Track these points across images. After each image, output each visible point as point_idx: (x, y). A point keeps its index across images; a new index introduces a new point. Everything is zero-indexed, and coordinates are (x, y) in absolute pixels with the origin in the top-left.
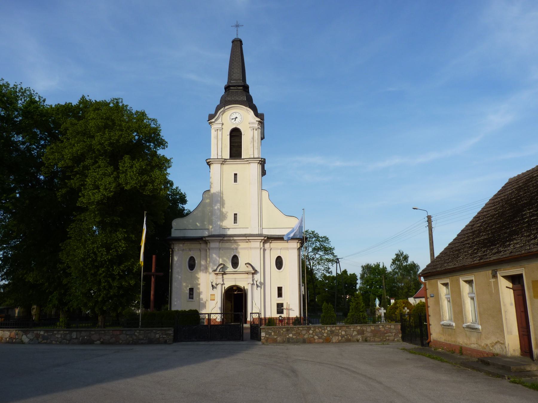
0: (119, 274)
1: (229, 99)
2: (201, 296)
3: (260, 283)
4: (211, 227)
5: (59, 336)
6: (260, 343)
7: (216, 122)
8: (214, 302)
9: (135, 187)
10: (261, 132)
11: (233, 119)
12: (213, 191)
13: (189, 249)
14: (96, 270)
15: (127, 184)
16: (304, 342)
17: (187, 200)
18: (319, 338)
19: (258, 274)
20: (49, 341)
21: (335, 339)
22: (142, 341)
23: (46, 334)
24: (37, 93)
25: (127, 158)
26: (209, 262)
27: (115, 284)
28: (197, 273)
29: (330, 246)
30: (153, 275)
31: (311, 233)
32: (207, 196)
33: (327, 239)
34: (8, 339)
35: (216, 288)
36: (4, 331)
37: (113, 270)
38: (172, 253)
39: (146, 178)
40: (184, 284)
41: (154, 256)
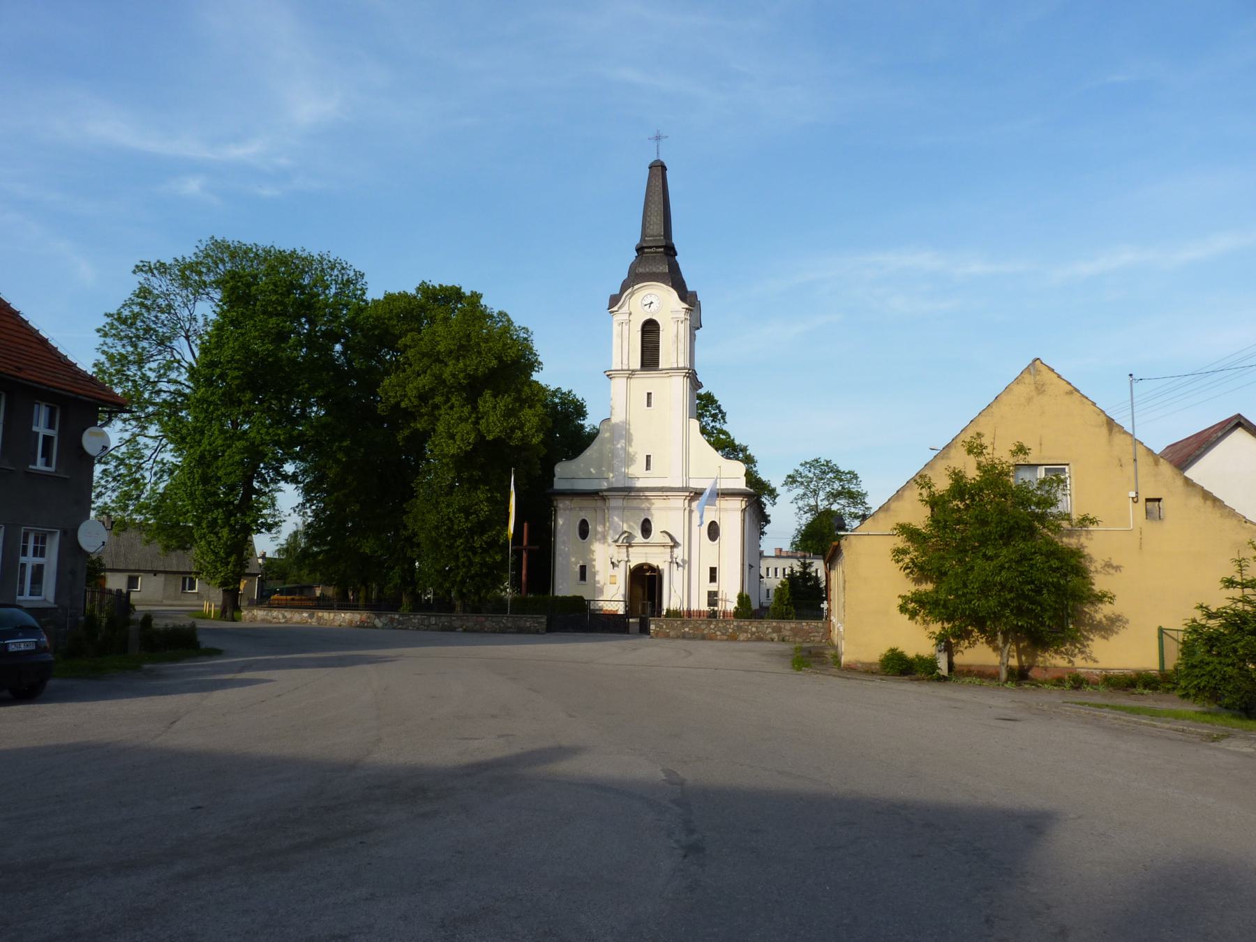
0: (481, 546)
1: (641, 270)
2: (598, 578)
3: (683, 560)
4: (611, 475)
5: (416, 621)
6: (648, 636)
7: (620, 311)
8: (616, 586)
9: (500, 437)
10: (690, 325)
11: (646, 305)
12: (615, 420)
13: (580, 508)
14: (452, 541)
15: (489, 432)
16: (704, 638)
17: (588, 412)
18: (723, 634)
19: (680, 547)
20: (405, 626)
21: (742, 637)
22: (511, 630)
23: (401, 619)
24: (351, 266)
25: (488, 394)
26: (609, 527)
27: (477, 560)
28: (591, 543)
29: (859, 490)
30: (525, 549)
31: (823, 465)
32: (606, 427)
33: (856, 477)
34: (358, 623)
35: (618, 566)
36: (353, 613)
37: (473, 542)
38: (555, 514)
39: (513, 421)
40: (573, 559)
41: (526, 524)
